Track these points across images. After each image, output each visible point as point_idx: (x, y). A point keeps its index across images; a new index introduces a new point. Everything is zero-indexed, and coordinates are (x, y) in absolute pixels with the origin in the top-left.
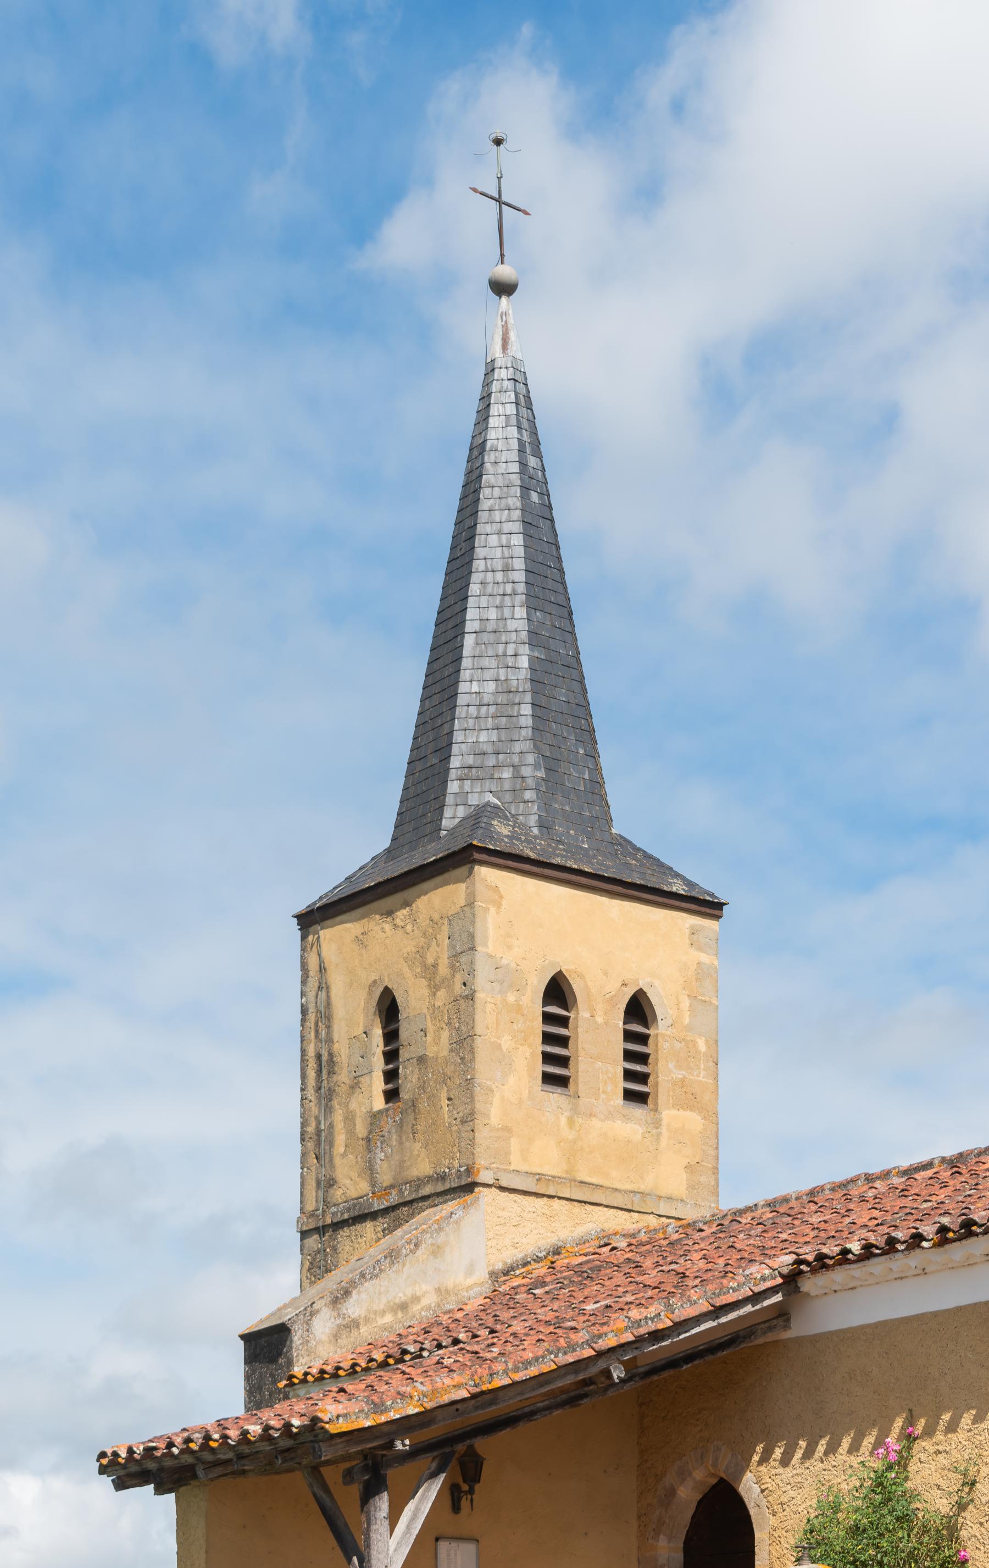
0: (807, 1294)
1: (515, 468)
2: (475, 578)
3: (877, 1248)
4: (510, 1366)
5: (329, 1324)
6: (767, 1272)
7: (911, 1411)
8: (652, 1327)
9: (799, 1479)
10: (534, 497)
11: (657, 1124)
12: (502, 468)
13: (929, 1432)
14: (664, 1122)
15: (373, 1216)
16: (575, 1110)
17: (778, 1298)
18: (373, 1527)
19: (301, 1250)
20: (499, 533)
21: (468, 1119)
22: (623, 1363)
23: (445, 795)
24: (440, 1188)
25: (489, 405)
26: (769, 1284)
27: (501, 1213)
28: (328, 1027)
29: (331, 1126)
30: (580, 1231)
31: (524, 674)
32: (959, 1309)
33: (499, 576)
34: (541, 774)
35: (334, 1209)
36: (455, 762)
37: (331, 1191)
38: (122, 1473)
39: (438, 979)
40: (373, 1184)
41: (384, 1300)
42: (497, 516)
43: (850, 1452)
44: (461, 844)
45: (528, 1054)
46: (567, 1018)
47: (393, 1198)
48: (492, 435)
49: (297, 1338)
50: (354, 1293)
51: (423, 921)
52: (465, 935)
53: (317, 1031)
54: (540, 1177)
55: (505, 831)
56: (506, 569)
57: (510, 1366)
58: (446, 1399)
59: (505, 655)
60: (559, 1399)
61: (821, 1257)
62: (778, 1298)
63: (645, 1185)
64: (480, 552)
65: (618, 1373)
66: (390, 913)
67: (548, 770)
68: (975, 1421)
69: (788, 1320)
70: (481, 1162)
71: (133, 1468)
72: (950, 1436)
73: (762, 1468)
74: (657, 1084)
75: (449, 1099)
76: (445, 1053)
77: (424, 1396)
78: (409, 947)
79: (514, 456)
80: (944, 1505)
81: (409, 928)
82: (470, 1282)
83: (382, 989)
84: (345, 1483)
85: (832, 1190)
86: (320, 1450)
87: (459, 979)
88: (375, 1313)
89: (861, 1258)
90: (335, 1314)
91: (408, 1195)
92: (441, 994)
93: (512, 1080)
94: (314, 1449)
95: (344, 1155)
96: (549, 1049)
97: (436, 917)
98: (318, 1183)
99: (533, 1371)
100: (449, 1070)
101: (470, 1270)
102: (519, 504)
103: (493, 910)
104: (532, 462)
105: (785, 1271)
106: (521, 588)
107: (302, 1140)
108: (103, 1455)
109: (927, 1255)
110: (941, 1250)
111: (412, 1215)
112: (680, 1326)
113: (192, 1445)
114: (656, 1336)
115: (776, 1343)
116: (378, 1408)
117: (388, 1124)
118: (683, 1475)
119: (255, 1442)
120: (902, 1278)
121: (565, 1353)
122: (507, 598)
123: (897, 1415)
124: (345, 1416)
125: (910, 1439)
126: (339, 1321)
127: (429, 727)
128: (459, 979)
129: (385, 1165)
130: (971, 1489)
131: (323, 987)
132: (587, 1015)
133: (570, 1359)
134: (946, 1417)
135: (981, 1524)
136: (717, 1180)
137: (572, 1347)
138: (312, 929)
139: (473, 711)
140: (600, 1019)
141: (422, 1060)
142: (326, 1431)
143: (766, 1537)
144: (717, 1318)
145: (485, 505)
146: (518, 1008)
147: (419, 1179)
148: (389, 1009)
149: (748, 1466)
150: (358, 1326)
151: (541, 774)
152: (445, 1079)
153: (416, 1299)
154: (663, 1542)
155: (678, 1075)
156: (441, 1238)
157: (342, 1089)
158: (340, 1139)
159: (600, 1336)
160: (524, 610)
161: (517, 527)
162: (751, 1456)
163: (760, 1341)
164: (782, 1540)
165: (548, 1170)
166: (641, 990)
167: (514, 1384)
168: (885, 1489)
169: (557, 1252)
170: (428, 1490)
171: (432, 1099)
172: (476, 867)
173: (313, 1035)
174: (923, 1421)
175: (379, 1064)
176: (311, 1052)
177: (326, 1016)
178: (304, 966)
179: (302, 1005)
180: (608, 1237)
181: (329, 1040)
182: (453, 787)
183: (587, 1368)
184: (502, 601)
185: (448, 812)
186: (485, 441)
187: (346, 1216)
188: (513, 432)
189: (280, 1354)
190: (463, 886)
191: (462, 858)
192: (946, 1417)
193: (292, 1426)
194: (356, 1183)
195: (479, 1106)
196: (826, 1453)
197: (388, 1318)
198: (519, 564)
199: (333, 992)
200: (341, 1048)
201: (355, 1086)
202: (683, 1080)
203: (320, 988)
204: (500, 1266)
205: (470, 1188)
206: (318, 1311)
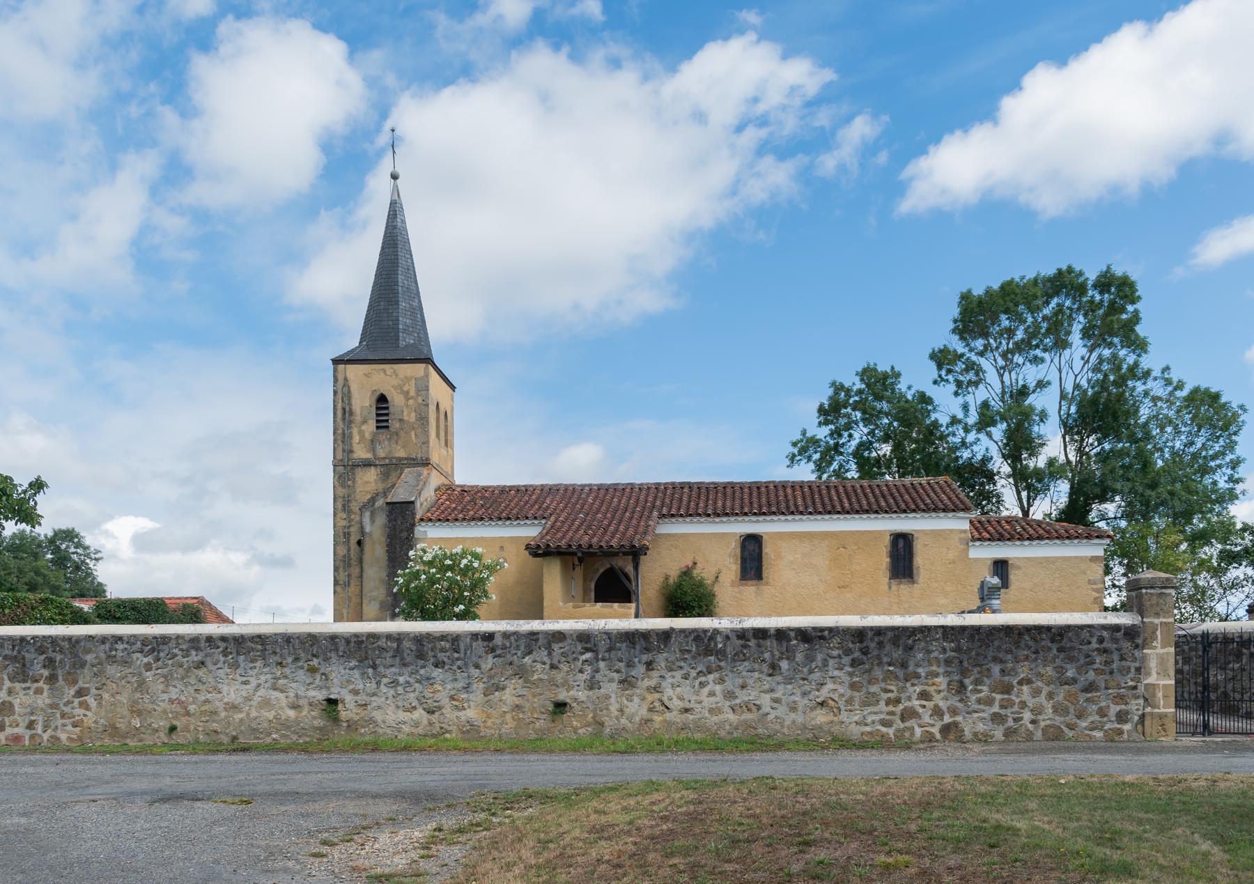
40: (374, 455)
141: (401, 420)
178: (335, 377)
181: (350, 404)
205: (428, 464)
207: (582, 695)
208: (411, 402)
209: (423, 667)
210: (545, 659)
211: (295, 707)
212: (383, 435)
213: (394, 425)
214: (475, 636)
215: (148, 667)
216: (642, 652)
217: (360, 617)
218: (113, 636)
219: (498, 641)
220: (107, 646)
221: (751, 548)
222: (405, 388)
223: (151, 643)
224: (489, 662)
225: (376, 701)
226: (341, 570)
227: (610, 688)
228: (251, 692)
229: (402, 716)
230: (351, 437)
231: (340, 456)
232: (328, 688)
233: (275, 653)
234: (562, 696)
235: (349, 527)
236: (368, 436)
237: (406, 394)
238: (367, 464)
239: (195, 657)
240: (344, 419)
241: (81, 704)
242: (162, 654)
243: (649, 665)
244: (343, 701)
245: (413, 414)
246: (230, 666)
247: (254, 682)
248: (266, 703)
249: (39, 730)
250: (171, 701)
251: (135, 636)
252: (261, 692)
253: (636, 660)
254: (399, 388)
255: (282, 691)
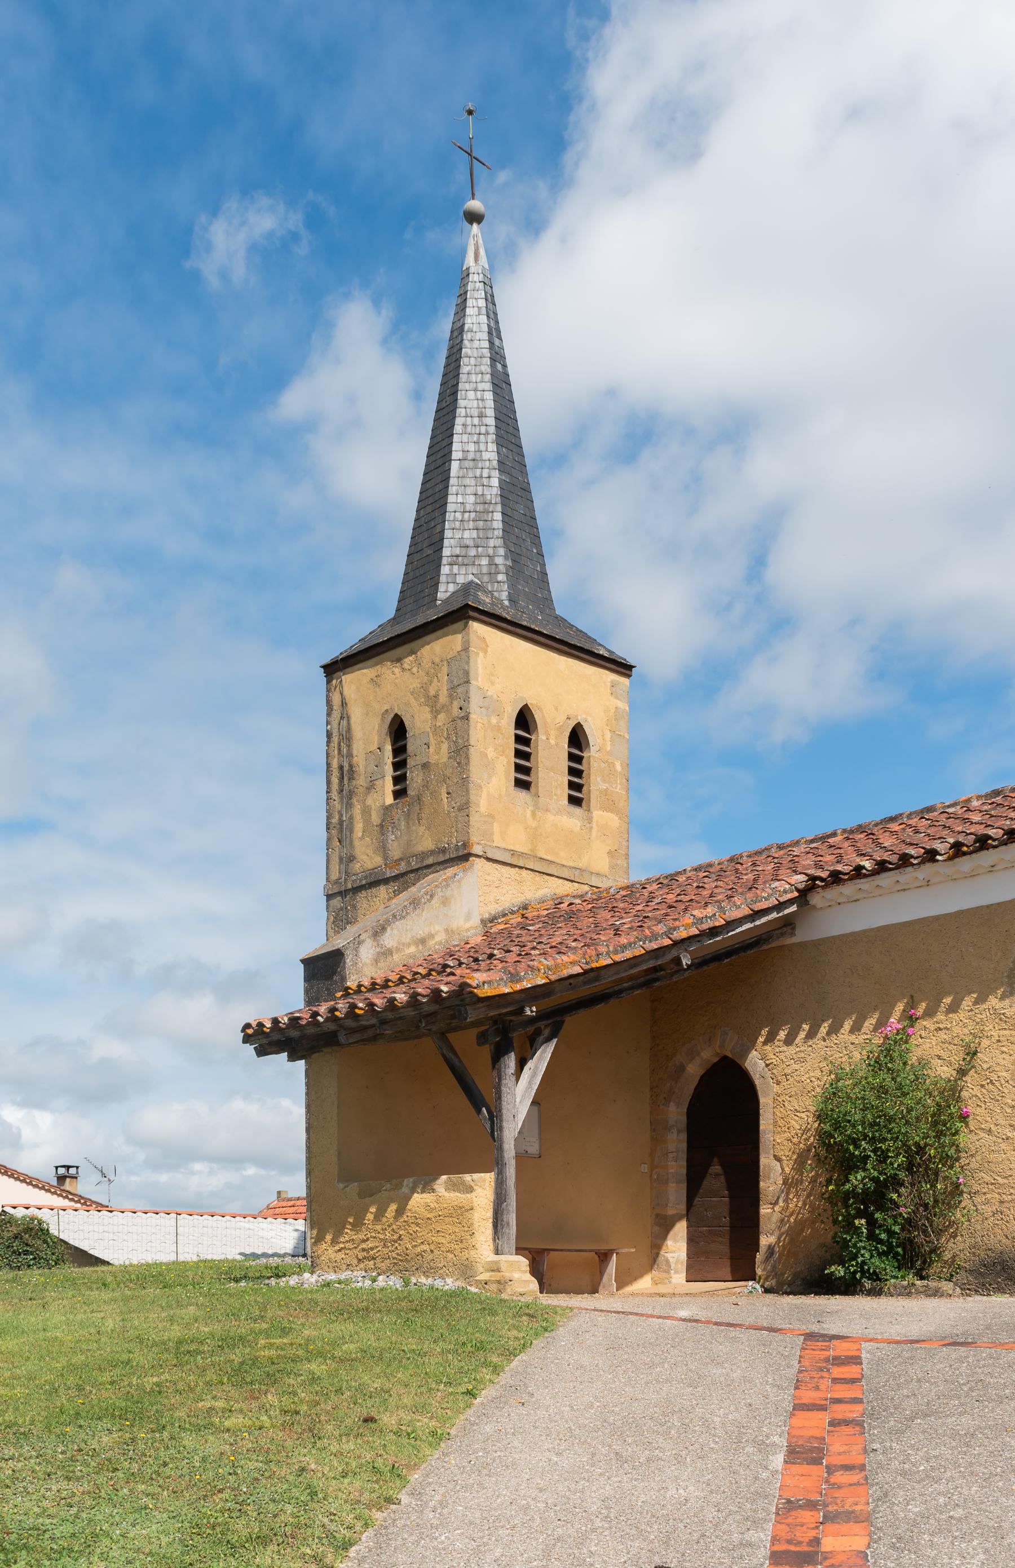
0: (814, 907)
1: (486, 344)
2: (459, 421)
3: (890, 863)
4: (611, 949)
5: (371, 951)
6: (787, 886)
7: (912, 997)
8: (710, 924)
9: (803, 1055)
10: (499, 367)
11: (590, 820)
12: (476, 344)
13: (930, 1013)
14: (595, 819)
15: (386, 881)
16: (536, 806)
17: (793, 908)
18: (504, 1082)
19: (327, 908)
20: (476, 390)
21: (464, 807)
22: (690, 952)
23: (439, 576)
24: (441, 858)
25: (466, 300)
26: (789, 896)
27: (487, 877)
28: (349, 746)
29: (351, 818)
30: (540, 894)
31: (496, 491)
32: (961, 913)
33: (476, 421)
34: (509, 563)
35: (354, 878)
36: (446, 552)
37: (351, 865)
38: (265, 1041)
39: (439, 706)
40: (386, 857)
41: (409, 936)
42: (473, 378)
43: (852, 1031)
44: (456, 606)
45: (505, 763)
46: (530, 740)
47: (403, 867)
48: (468, 320)
49: (348, 961)
50: (389, 929)
51: (426, 663)
52: (461, 673)
53: (339, 750)
54: (513, 853)
55: (488, 600)
56: (481, 416)
57: (611, 949)
58: (566, 973)
59: (481, 477)
60: (639, 981)
61: (859, 868)
62: (793, 908)
63: (582, 864)
64: (461, 403)
65: (686, 961)
66: (399, 660)
67: (514, 561)
68: (976, 1002)
69: (793, 929)
70: (474, 839)
71: (276, 1037)
72: (951, 1015)
73: (767, 1047)
74: (589, 791)
75: (448, 793)
76: (445, 760)
77: (549, 969)
78: (415, 684)
79: (485, 336)
80: (945, 1072)
81: (415, 670)
82: (468, 925)
83: (392, 716)
84: (479, 1044)
85: (749, 856)
86: (467, 1013)
87: (456, 704)
88: (403, 944)
89: (874, 873)
90: (375, 944)
91: (414, 865)
92: (442, 716)
93: (494, 780)
94: (460, 1011)
95: (362, 838)
96: (518, 761)
97: (437, 660)
98: (341, 859)
99: (628, 954)
100: (448, 772)
101: (468, 918)
102: (489, 370)
103: (481, 654)
104: (497, 342)
105: (801, 886)
106: (492, 429)
107: (328, 829)
108: (248, 1026)
109: (940, 869)
110: (951, 862)
111: (419, 880)
112: (731, 924)
113: (337, 1013)
114: (713, 931)
115: (781, 947)
116: (514, 978)
117: (398, 814)
118: (692, 1054)
119: (403, 1007)
120: (905, 890)
121: (650, 941)
122: (482, 437)
123: (899, 1000)
124: (489, 982)
125: (912, 1020)
126: (378, 950)
127: (424, 528)
128: (456, 704)
129: (395, 844)
130: (972, 1058)
131: (345, 716)
132: (544, 738)
133: (654, 945)
134: (948, 1000)
135: (982, 1086)
136: (628, 863)
137: (655, 937)
138: (335, 675)
139: (458, 515)
140: (553, 742)
141: (425, 766)
142: (476, 995)
143: (770, 1102)
144: (754, 921)
145: (464, 369)
146: (498, 728)
147: (423, 853)
148: (398, 731)
149: (754, 1046)
150: (392, 954)
151: (509, 563)
152: (445, 779)
153: (431, 936)
154: (672, 1107)
155: (604, 786)
156: (448, 892)
157: (361, 790)
158: (359, 827)
159: (675, 929)
160: (495, 445)
161: (488, 386)
162: (757, 1038)
163: (774, 945)
164: (786, 1104)
165: (518, 848)
166: (579, 723)
167: (616, 963)
168: (887, 1058)
169: (525, 907)
170: (544, 1052)
171: (434, 794)
172: (470, 622)
173: (336, 752)
174: (924, 1004)
175: (389, 771)
176: (335, 764)
177: (347, 737)
178: (329, 702)
179: (327, 731)
180: (561, 898)
181: (350, 755)
182: (445, 570)
183: (664, 955)
184: (479, 439)
185: (442, 588)
186: (464, 324)
187: (364, 882)
188: (484, 319)
189: (334, 973)
190: (459, 636)
191: (462, 613)
192: (948, 1000)
193: (442, 991)
194: (371, 858)
195: (472, 798)
196: (828, 1034)
197: (412, 949)
198: (491, 412)
199: (353, 720)
200: (360, 760)
201: (371, 787)
202: (606, 790)
203: (342, 718)
204: (486, 916)
205: (466, 857)
206: (363, 941)
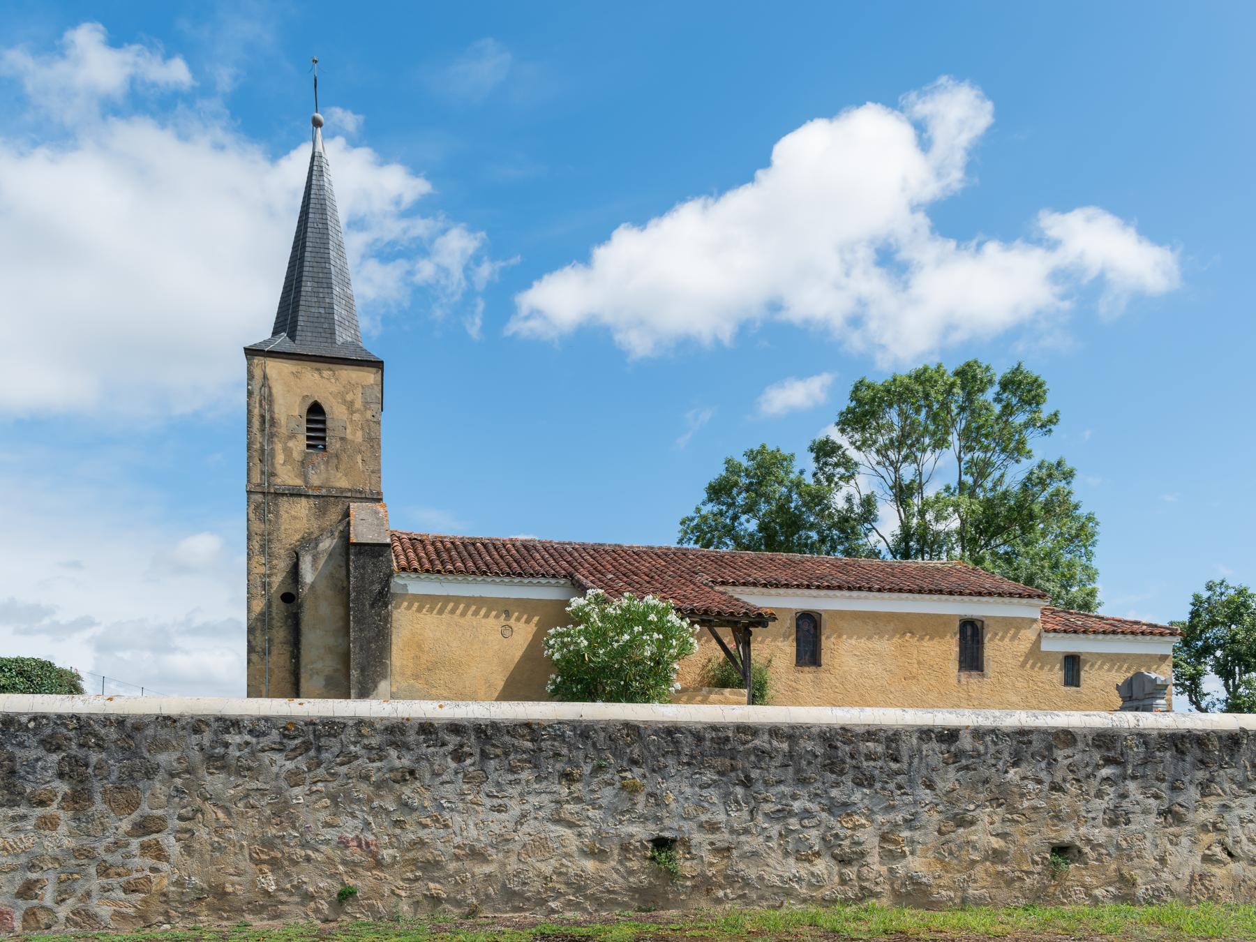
40: (306, 482)
181: (271, 411)
207: (1100, 834)
208: (356, 417)
209: (837, 784)
210: (1043, 775)
211: (597, 854)
212: (317, 457)
213: (333, 444)
214: (925, 733)
215: (295, 779)
216: (1195, 767)
217: (296, 692)
218: (219, 719)
219: (966, 742)
220: (207, 738)
221: (806, 627)
222: (349, 397)
223: (301, 733)
224: (949, 779)
225: (752, 842)
226: (258, 633)
227: (1145, 823)
228: (511, 826)
229: (793, 867)
230: (272, 454)
231: (256, 479)
232: (658, 819)
233: (557, 755)
234: (1067, 834)
235: (269, 576)
236: (297, 456)
237: (350, 406)
238: (295, 494)
239: (398, 760)
240: (263, 430)
241: (144, 848)
242: (325, 755)
243: (1205, 788)
244: (686, 844)
245: (359, 433)
246: (468, 779)
247: (515, 809)
248: (540, 845)
249: (48, 898)
250: (343, 844)
251: (267, 719)
252: (529, 827)
253: (1186, 779)
254: (342, 395)
255: (570, 825)
